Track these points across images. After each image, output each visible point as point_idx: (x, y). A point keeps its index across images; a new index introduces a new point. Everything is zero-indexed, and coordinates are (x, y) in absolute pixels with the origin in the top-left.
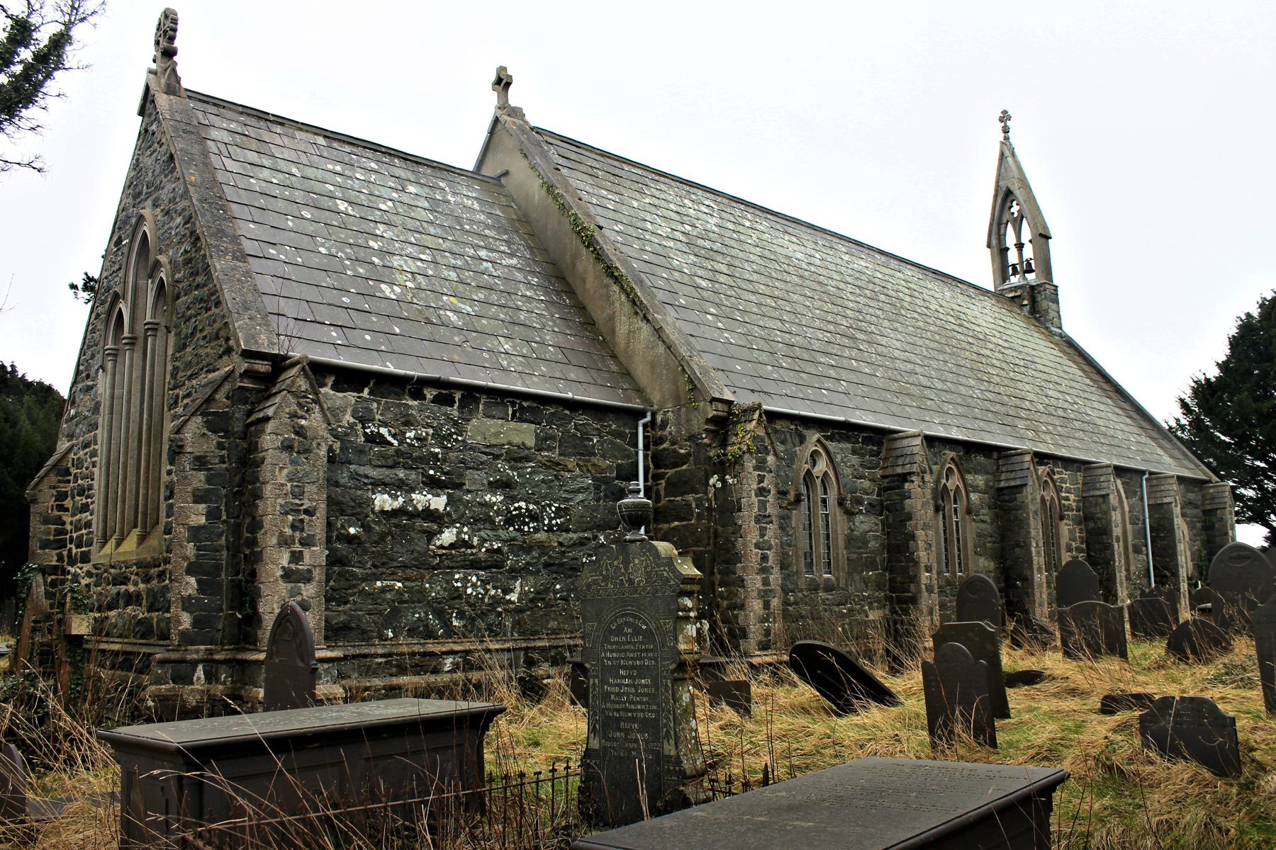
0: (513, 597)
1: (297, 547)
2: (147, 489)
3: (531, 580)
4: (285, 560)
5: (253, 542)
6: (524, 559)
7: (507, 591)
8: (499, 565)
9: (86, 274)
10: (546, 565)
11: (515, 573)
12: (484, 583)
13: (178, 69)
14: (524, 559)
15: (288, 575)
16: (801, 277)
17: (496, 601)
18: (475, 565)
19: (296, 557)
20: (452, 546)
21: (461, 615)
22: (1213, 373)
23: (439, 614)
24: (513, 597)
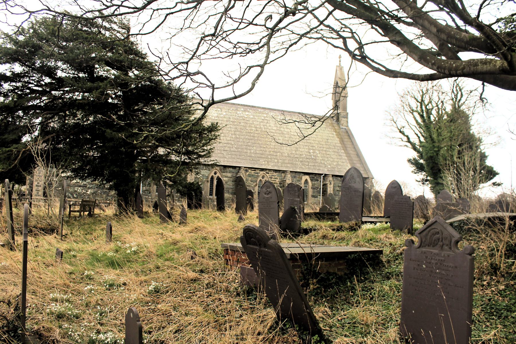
0: (88, 193)
1: (38, 182)
2: (371, 217)
3: (93, 190)
4: (36, 183)
5: (324, 218)
6: (91, 186)
7: (87, 191)
8: (86, 187)
9: (502, 184)
10: (97, 187)
11: (89, 188)
12: (82, 190)
13: (348, 54)
14: (91, 186)
15: (37, 186)
16: (343, 162)
17: (84, 193)
18: (80, 186)
19: (38, 183)
20: (75, 183)
21: (76, 195)
22: (405, 192)
23: (72, 194)
24: (88, 193)
